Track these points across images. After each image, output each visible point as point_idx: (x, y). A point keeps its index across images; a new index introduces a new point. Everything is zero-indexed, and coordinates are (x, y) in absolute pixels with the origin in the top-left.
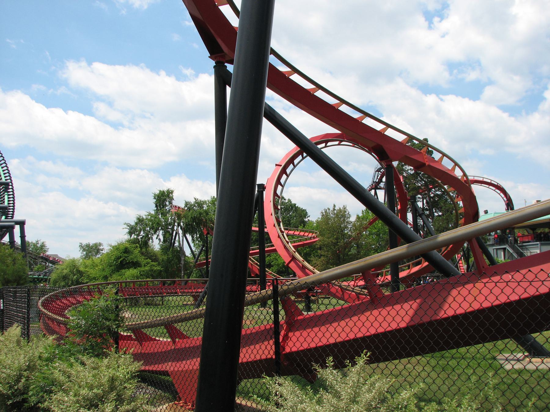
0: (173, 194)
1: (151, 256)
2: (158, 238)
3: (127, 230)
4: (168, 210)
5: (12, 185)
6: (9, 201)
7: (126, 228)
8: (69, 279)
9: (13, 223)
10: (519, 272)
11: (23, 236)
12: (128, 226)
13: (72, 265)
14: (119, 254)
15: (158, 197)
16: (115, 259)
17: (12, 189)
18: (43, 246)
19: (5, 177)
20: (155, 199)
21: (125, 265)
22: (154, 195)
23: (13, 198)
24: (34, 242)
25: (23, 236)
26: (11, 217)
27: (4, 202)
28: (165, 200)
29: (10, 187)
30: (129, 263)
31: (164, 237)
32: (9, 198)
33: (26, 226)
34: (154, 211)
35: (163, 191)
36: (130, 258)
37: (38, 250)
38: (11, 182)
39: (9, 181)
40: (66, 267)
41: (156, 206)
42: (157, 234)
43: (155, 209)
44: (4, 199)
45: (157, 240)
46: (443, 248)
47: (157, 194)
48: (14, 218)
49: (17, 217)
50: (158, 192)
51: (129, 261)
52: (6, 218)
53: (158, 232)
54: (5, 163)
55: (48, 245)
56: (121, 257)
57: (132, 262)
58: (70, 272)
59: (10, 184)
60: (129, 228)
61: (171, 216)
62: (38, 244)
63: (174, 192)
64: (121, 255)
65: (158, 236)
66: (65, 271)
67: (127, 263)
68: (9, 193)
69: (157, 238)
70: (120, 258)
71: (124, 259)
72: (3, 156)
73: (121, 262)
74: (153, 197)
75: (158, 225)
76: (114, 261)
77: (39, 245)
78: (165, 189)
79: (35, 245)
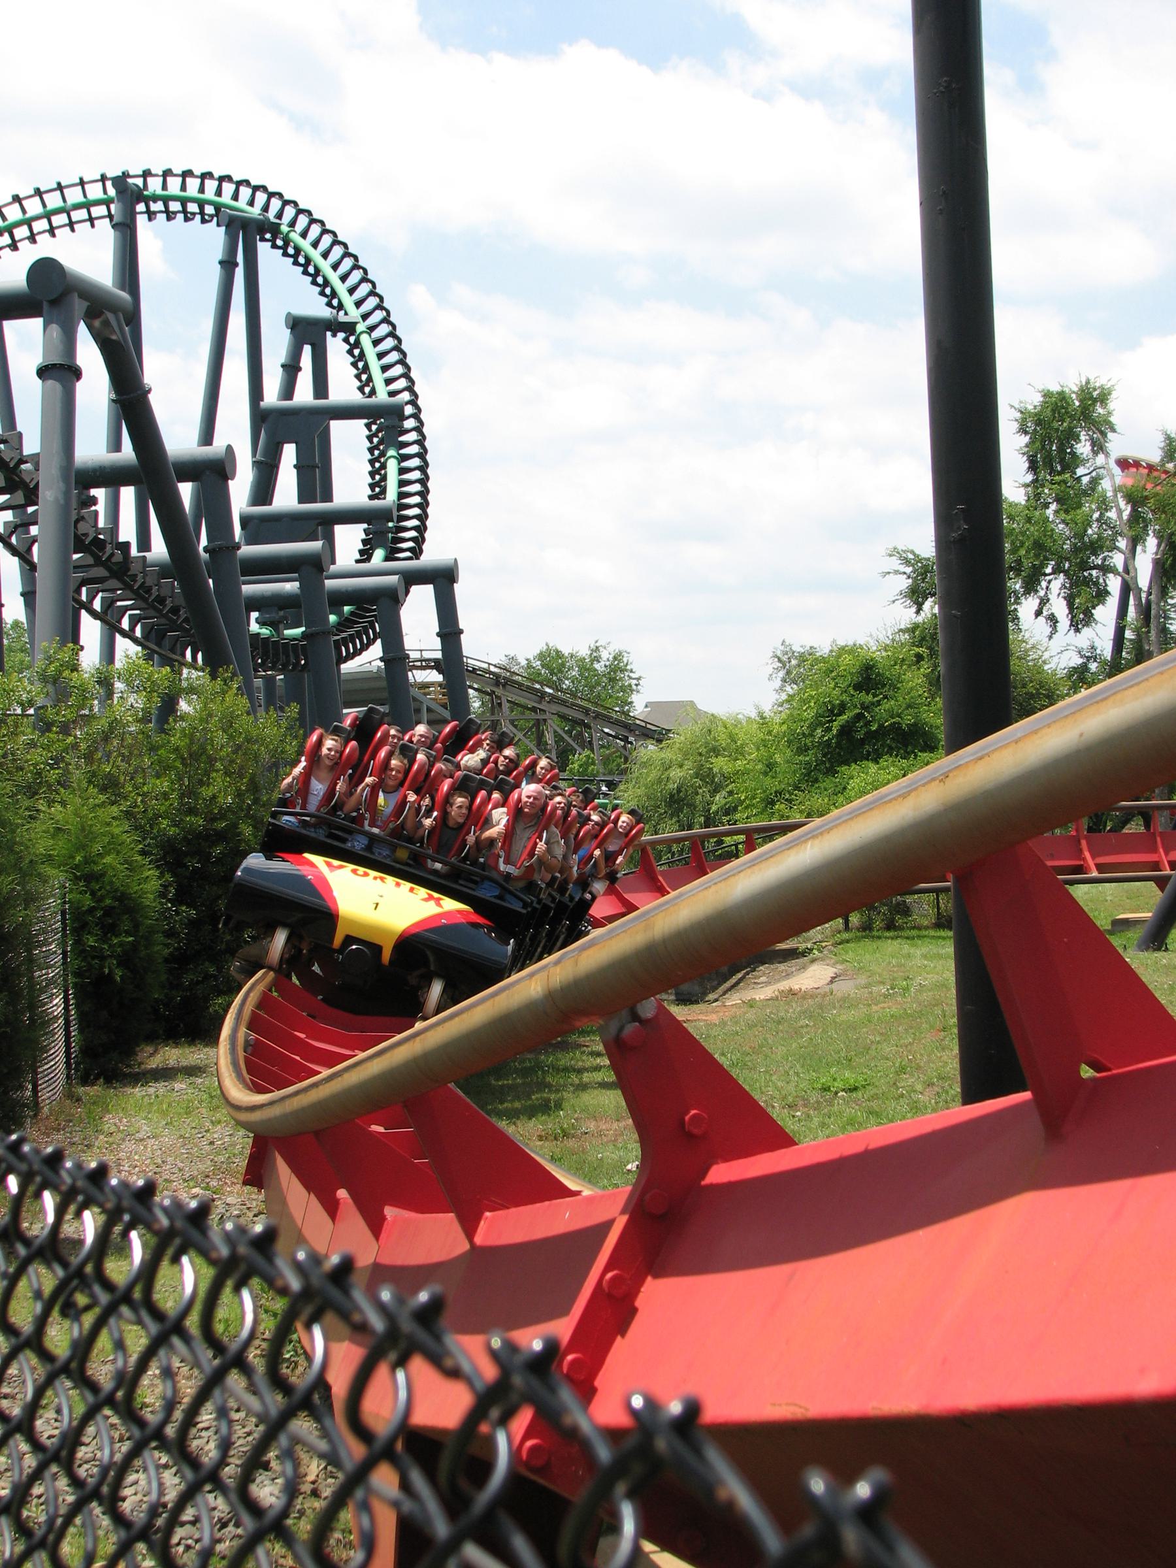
0: (1112, 405)
1: (1032, 696)
2: (1045, 613)
3: (904, 583)
4: (1085, 480)
5: (416, 416)
6: (402, 483)
7: (897, 572)
8: (692, 806)
9: (393, 579)
10: (1069, 630)
11: (450, 632)
12: (907, 562)
13: (707, 744)
14: (836, 692)
15: (1039, 422)
16: (818, 715)
17: (419, 429)
18: (618, 667)
19: (388, 382)
20: (1026, 433)
21: (862, 742)
22: (1018, 415)
23: (423, 469)
24: (584, 652)
25: (450, 632)
26: (408, 554)
27: (384, 491)
28: (1071, 436)
29: (410, 424)
30: (882, 732)
31: (1070, 606)
32: (402, 471)
33: (460, 589)
34: (1022, 491)
35: (1062, 396)
36: (886, 710)
37: (598, 683)
38: (413, 402)
39: (406, 396)
40: (680, 757)
41: (1033, 467)
42: (1042, 593)
43: (1029, 477)
44: (384, 478)
45: (1041, 619)
46: (34, 1464)
47: (1030, 407)
48: (422, 558)
49: (433, 554)
50: (1037, 399)
51: (881, 726)
52: (387, 559)
53: (1044, 584)
54: (386, 320)
55: (638, 663)
56: (843, 708)
57: (896, 728)
58: (697, 775)
59: (409, 410)
60: (909, 570)
61: (1099, 509)
62: (597, 659)
63: (1114, 395)
64: (844, 697)
65: (1044, 601)
66: (676, 774)
67: (871, 735)
68: (403, 451)
69: (1038, 613)
70: (840, 714)
71: (859, 717)
72: (378, 291)
73: (846, 731)
74: (1016, 426)
75: (1037, 556)
76: (813, 727)
77: (602, 663)
78: (1072, 384)
79: (585, 667)
